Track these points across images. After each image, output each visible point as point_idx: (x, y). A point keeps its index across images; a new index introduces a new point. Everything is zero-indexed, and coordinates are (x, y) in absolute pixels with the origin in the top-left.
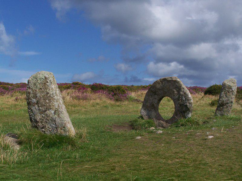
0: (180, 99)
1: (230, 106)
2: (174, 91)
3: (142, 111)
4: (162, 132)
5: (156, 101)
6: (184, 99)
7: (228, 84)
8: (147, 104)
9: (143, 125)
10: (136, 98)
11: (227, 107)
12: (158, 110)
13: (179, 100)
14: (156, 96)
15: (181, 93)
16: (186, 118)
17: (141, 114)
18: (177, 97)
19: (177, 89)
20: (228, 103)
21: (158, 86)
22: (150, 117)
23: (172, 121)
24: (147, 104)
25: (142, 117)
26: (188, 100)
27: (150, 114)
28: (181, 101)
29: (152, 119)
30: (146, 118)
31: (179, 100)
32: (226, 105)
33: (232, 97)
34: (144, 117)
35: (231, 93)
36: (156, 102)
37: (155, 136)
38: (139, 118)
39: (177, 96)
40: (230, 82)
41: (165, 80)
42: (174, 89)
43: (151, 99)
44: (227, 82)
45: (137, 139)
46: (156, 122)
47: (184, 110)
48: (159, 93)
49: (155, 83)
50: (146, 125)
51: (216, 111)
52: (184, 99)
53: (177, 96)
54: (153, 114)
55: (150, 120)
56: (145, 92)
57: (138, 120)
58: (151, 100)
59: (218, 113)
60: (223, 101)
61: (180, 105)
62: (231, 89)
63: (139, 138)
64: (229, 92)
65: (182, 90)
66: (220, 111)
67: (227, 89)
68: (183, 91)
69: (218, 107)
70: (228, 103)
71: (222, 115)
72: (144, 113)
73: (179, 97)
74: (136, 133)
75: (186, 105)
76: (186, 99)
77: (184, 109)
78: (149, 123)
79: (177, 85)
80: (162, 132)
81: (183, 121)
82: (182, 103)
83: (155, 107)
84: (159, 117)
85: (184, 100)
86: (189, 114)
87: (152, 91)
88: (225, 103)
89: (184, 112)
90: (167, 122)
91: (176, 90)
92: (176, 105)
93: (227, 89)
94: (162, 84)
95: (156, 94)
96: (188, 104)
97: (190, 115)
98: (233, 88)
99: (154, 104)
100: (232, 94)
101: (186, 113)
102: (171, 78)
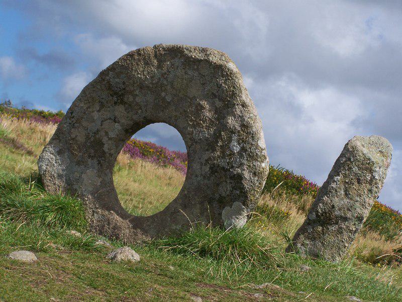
0: (220, 144)
1: (351, 231)
2: (202, 108)
3: (48, 155)
4: (137, 257)
5: (115, 130)
6: (236, 149)
7: (365, 151)
8: (75, 133)
9: (35, 210)
10: (13, 136)
11: (340, 231)
12: (111, 166)
13: (211, 145)
14: (120, 111)
15: (231, 121)
16: (222, 228)
17: (40, 167)
18: (207, 133)
19: (219, 104)
20: (345, 219)
21: (141, 72)
22: (71, 189)
23: (161, 227)
24: (75, 133)
25: (39, 180)
26: (253, 157)
27: (77, 175)
28: (223, 152)
29: (82, 196)
30: (55, 187)
31: (214, 150)
32: (337, 223)
33: (367, 200)
34: (47, 181)
35: (365, 187)
36: (112, 135)
37: (105, 267)
38: (26, 181)
39: (208, 128)
40: (373, 149)
41: (175, 52)
42: (206, 97)
43: (96, 115)
44: (363, 146)
45: (14, 262)
46: (93, 215)
47: (224, 194)
48: (138, 99)
49: (131, 55)
50: (50, 217)
51: (297, 236)
52: (236, 149)
53: (208, 128)
54: (90, 177)
55: (70, 200)
56: (51, 129)
57: (23, 187)
58: (93, 121)
59: (304, 246)
60: (333, 207)
61: (214, 169)
62: (371, 171)
63: (27, 256)
64: (359, 182)
65: (238, 110)
66: (313, 239)
67: (355, 169)
68: (242, 117)
69: (309, 224)
70: (345, 219)
71: (316, 256)
72: (53, 165)
73: (217, 136)
74: (11, 231)
75: (240, 177)
76: (243, 149)
77: (225, 189)
78: (61, 208)
79: (219, 86)
80: (137, 257)
81: (212, 236)
82: (222, 163)
83: (104, 153)
84: (107, 197)
85: (232, 154)
86: (239, 213)
87: (110, 87)
88: (336, 217)
89: (223, 202)
90: (138, 223)
91: (212, 104)
92: (196, 166)
93: (355, 169)
94: (159, 67)
95: (123, 102)
96: (246, 174)
97: (241, 222)
98: (377, 169)
99: (105, 140)
100: (370, 191)
101: (227, 208)
102: (204, 50)
